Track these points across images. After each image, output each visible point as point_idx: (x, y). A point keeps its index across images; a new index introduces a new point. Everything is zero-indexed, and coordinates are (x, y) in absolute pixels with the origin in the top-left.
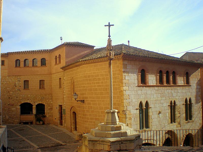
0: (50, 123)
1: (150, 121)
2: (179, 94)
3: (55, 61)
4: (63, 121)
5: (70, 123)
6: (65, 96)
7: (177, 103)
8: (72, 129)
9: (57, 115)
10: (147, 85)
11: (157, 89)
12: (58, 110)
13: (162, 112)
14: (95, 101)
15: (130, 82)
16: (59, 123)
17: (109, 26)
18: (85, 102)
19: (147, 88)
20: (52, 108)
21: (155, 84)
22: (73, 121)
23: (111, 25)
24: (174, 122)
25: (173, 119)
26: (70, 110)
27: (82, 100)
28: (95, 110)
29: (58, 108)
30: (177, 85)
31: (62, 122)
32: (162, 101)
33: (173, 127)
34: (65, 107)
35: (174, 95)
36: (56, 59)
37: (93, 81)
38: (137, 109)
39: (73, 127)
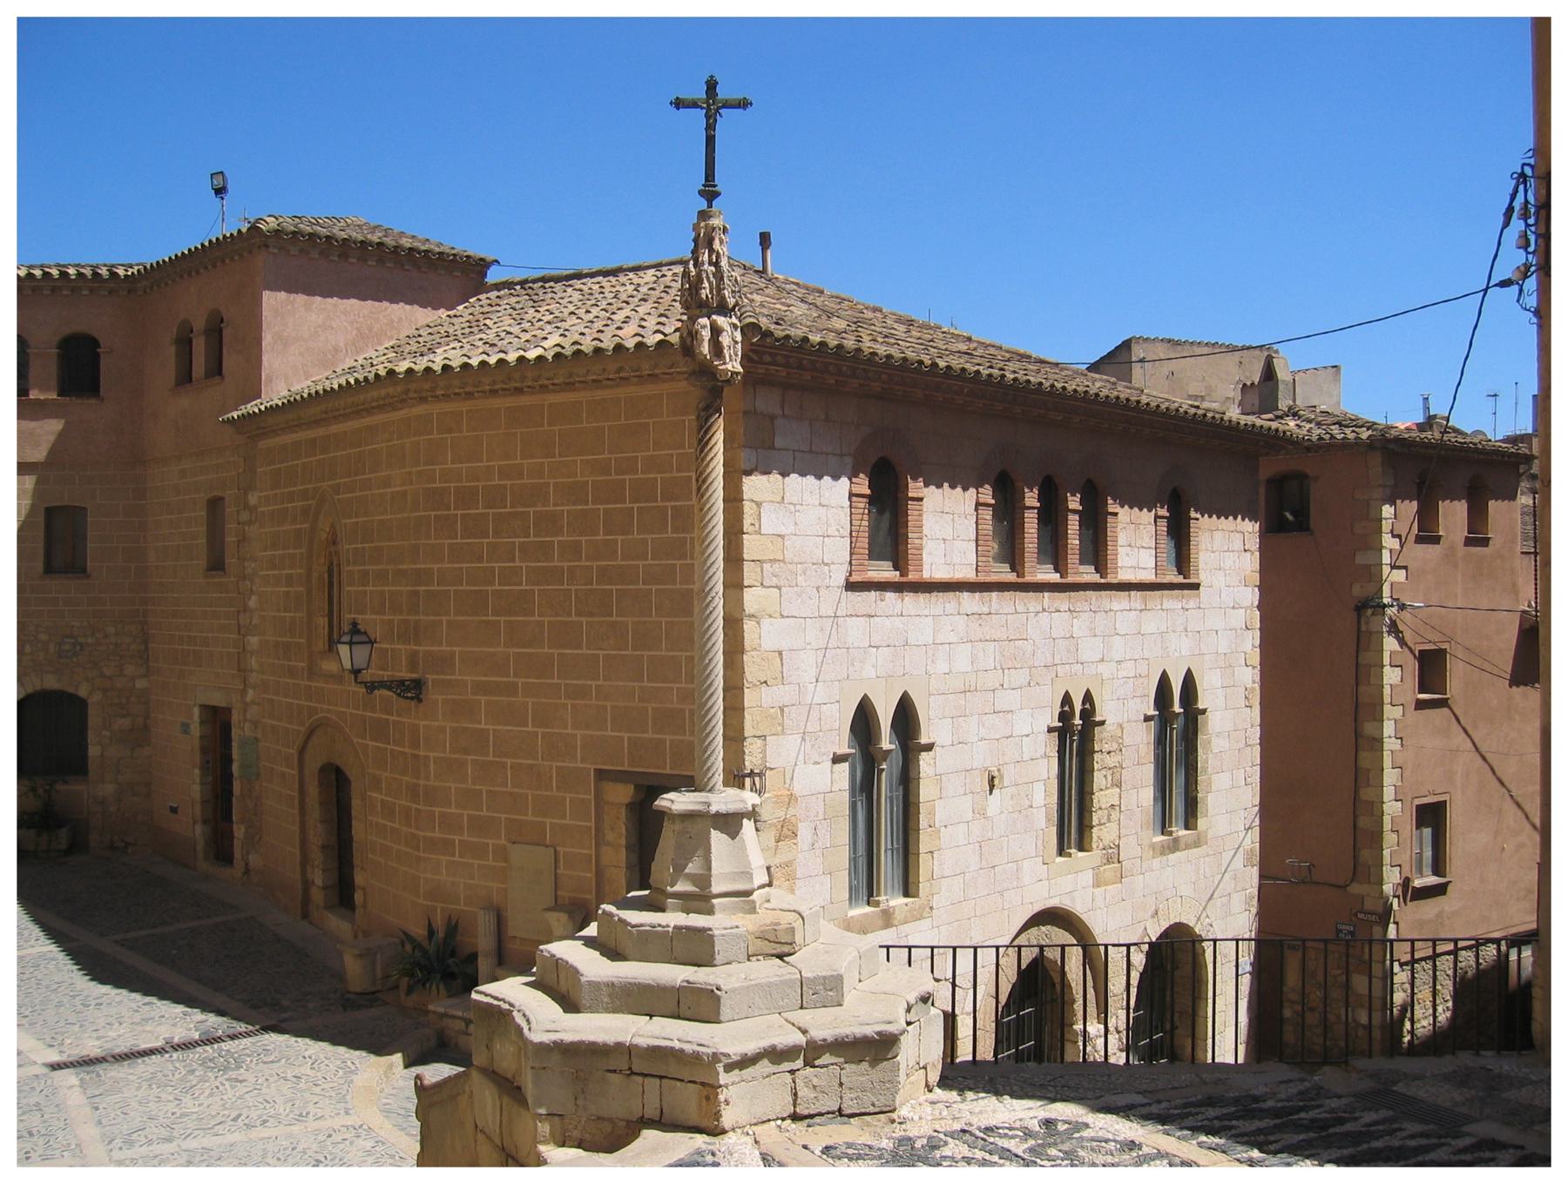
0: (128, 845)
1: (925, 842)
2: (1118, 648)
3: (173, 360)
4: (239, 831)
5: (297, 851)
6: (254, 641)
7: (1105, 710)
8: (317, 896)
9: (187, 785)
10: (912, 577)
11: (976, 610)
12: (197, 743)
13: (1002, 777)
14: (511, 689)
15: (789, 556)
16: (200, 846)
17: (712, 103)
18: (433, 695)
19: (910, 601)
20: (146, 727)
21: (968, 574)
22: (318, 835)
23: (727, 105)
24: (1081, 849)
25: (1074, 822)
26: (294, 752)
27: (402, 682)
28: (509, 761)
29: (196, 730)
30: (1111, 579)
31: (232, 837)
32: (1005, 699)
33: (1072, 884)
34: (255, 724)
35: (1085, 655)
36: (184, 343)
37: (496, 534)
38: (837, 759)
39: (318, 878)
